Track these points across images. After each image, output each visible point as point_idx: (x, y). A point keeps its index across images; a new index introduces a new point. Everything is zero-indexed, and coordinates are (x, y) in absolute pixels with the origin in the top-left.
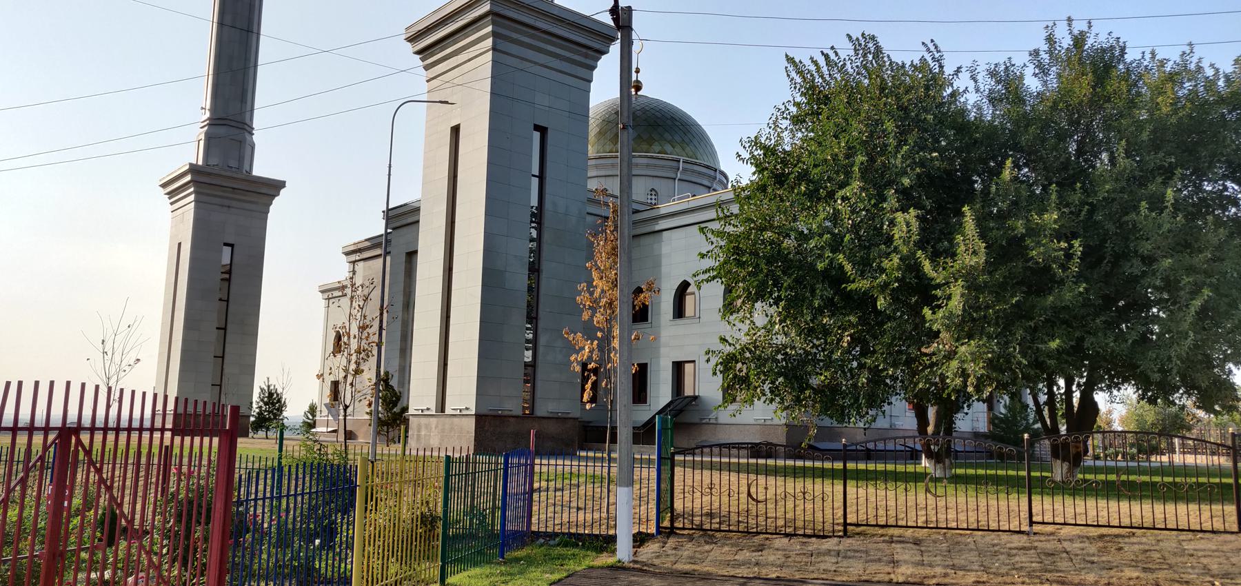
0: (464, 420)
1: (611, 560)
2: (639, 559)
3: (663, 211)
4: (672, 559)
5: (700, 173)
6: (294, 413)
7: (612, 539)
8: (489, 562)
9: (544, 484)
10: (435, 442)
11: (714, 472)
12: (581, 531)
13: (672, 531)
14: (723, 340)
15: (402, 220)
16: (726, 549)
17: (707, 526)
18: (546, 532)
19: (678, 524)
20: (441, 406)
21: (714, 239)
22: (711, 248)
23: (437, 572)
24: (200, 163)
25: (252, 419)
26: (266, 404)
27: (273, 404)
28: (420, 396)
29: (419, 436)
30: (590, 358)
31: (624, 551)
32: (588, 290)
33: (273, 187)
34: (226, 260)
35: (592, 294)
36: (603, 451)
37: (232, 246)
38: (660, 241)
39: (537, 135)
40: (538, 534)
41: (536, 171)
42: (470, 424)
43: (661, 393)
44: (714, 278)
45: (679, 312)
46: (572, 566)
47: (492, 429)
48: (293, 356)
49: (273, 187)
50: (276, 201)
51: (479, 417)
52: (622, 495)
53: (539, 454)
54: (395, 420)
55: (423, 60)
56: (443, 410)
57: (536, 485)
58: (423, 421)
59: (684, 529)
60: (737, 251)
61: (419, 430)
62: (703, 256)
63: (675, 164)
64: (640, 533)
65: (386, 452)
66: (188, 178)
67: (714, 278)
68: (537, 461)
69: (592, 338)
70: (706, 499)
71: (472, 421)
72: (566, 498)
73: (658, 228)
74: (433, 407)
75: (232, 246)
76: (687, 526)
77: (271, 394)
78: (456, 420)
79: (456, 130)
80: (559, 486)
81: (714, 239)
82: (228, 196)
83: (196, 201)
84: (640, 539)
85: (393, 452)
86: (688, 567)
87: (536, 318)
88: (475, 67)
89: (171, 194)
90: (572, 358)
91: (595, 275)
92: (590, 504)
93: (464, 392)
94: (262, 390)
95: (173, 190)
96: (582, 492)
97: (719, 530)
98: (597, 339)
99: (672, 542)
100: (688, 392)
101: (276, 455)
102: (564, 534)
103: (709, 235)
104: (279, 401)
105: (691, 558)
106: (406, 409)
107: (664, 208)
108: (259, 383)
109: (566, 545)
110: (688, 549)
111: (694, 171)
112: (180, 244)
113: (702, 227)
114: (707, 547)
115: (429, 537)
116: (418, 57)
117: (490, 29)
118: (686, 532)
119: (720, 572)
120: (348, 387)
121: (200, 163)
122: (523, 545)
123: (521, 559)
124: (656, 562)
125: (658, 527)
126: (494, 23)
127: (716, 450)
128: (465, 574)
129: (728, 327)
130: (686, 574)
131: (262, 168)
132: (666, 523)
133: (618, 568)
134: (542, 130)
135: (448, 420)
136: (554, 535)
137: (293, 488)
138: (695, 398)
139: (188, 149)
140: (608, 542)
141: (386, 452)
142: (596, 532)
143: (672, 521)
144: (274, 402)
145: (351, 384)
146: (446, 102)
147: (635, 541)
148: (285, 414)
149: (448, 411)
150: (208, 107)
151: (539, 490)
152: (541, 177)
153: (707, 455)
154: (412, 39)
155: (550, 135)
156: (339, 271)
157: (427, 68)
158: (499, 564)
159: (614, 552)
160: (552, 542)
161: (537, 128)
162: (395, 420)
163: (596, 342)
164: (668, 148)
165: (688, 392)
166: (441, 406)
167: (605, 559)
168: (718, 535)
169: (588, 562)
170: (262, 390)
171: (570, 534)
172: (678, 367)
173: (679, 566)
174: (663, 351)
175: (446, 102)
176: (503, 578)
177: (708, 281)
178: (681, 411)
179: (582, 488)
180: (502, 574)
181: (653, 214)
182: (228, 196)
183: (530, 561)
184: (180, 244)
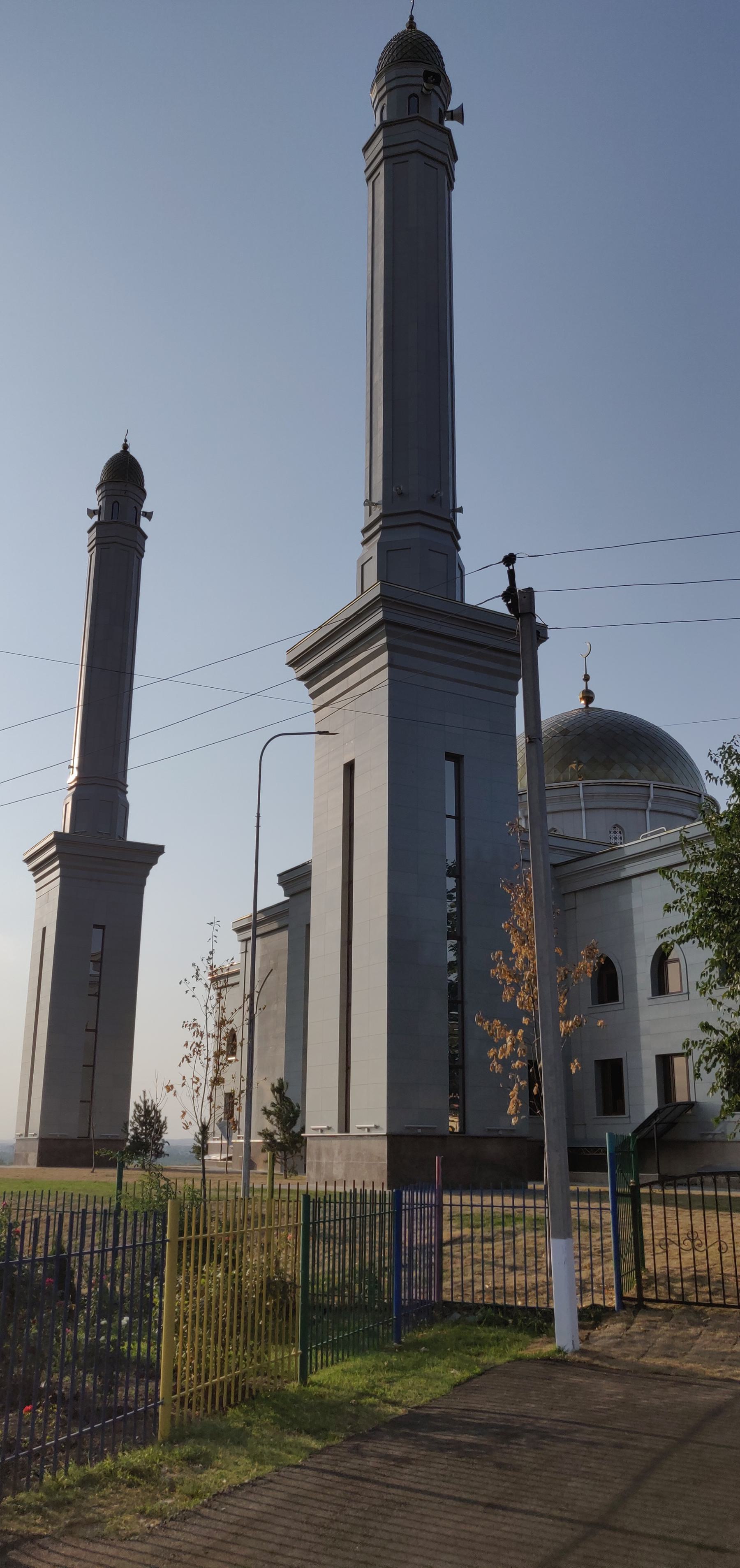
0: (373, 1141)
1: (548, 1349)
2: (590, 1348)
3: (628, 852)
4: (639, 1348)
5: (678, 801)
6: (178, 1134)
7: (548, 1315)
8: (380, 1348)
9: (467, 1231)
10: (338, 1172)
11: (708, 1213)
12: (510, 1302)
13: (639, 1305)
14: (706, 1027)
15: (296, 881)
16: (721, 1334)
17: (692, 1298)
18: (462, 1303)
19: (650, 1294)
20: (26, 1135)
21: (683, 885)
22: (678, 896)
23: (295, 1365)
24: (67, 831)
25: (128, 1144)
26: (142, 1124)
27: (150, 1124)
28: (320, 1115)
29: (319, 1165)
30: (514, 1056)
31: (565, 1334)
32: (506, 960)
33: (153, 853)
34: (96, 948)
35: (511, 964)
36: (603, 1183)
37: (103, 927)
38: (630, 891)
39: (450, 766)
40: (451, 1306)
41: (451, 810)
42: (382, 1148)
43: (645, 1100)
44: (688, 937)
45: (660, 986)
46: (490, 1358)
47: (410, 1153)
48: (168, 1061)
49: (153, 853)
50: (154, 871)
51: (393, 1139)
52: (558, 1252)
53: (451, 1186)
54: (294, 1143)
55: (308, 686)
56: (347, 1130)
57: (446, 1237)
58: (324, 1143)
59: (657, 1301)
60: (715, 898)
61: (319, 1156)
62: (668, 908)
63: (643, 791)
64: (594, 1306)
65: (285, 1187)
66: (53, 850)
67: (688, 937)
68: (446, 1199)
69: (515, 1025)
70: (687, 1257)
71: (384, 1144)
72: (498, 1252)
73: (624, 874)
74: (335, 1125)
75: (103, 927)
76: (664, 1296)
77: (148, 1112)
78: (364, 1143)
79: (350, 767)
80: (487, 1234)
81: (683, 885)
82: (99, 869)
83: (62, 876)
84: (591, 1317)
85: (294, 1187)
86: (660, 1362)
87: (462, 1002)
88: (369, 687)
89: (36, 870)
90: (491, 1054)
91: (514, 940)
92: (531, 1260)
93: (372, 1109)
94: (137, 1106)
95: (37, 864)
96: (520, 1243)
97: (711, 1305)
98: (523, 1026)
99: (639, 1324)
100: (681, 1096)
101: (113, 1191)
102: (486, 1306)
103: (677, 880)
104: (158, 1120)
105: (669, 1347)
106: (303, 1130)
107: (631, 847)
108: (135, 1097)
109: (489, 1324)
110: (665, 1331)
111: (670, 799)
112: (44, 929)
113: (664, 871)
114: (692, 1331)
115: (284, 1309)
116: (303, 683)
117: (384, 640)
118: (660, 1306)
119: (710, 1372)
120: (207, 1102)
121: (67, 831)
122: (432, 1322)
123: (424, 1344)
124: (616, 1352)
125: (620, 1296)
126: (388, 634)
127: (722, 1179)
128: (338, 1368)
129: (713, 1008)
130: (658, 1374)
131: (138, 831)
132: (632, 1293)
133: (557, 1361)
134: (456, 759)
135: (353, 1143)
136: (472, 1308)
137: (121, 1241)
138: (691, 1105)
139: (55, 816)
140: (541, 1321)
141: (285, 1187)
142: (532, 1303)
143: (640, 1289)
144: (151, 1120)
145: (210, 1098)
146: (326, 733)
147: (580, 1318)
148: (165, 1137)
149: (353, 1131)
150: (76, 763)
151: (452, 1242)
152: (459, 818)
153: (723, 1187)
154: (295, 663)
155: (467, 764)
156: (230, 952)
157: (313, 696)
158: (391, 1351)
159: (551, 1335)
160: (471, 1318)
161: (449, 756)
162: (294, 1143)
163: (520, 1032)
164: (633, 771)
165: (681, 1096)
166: (345, 1125)
167: (541, 1348)
168: (709, 1310)
169: (515, 1351)
170: (137, 1106)
171: (496, 1307)
172: (665, 1063)
173: (649, 1361)
174: (644, 1040)
175: (326, 733)
176: (390, 1375)
177: (680, 942)
178: (673, 1124)
179: (520, 1237)
180: (390, 1368)
181: (614, 856)
182: (99, 869)
183: (435, 1348)
184: (44, 929)
